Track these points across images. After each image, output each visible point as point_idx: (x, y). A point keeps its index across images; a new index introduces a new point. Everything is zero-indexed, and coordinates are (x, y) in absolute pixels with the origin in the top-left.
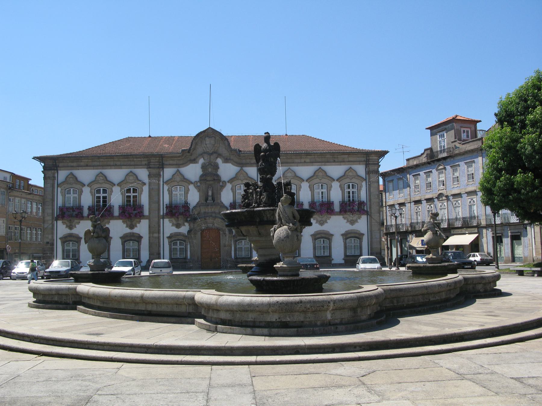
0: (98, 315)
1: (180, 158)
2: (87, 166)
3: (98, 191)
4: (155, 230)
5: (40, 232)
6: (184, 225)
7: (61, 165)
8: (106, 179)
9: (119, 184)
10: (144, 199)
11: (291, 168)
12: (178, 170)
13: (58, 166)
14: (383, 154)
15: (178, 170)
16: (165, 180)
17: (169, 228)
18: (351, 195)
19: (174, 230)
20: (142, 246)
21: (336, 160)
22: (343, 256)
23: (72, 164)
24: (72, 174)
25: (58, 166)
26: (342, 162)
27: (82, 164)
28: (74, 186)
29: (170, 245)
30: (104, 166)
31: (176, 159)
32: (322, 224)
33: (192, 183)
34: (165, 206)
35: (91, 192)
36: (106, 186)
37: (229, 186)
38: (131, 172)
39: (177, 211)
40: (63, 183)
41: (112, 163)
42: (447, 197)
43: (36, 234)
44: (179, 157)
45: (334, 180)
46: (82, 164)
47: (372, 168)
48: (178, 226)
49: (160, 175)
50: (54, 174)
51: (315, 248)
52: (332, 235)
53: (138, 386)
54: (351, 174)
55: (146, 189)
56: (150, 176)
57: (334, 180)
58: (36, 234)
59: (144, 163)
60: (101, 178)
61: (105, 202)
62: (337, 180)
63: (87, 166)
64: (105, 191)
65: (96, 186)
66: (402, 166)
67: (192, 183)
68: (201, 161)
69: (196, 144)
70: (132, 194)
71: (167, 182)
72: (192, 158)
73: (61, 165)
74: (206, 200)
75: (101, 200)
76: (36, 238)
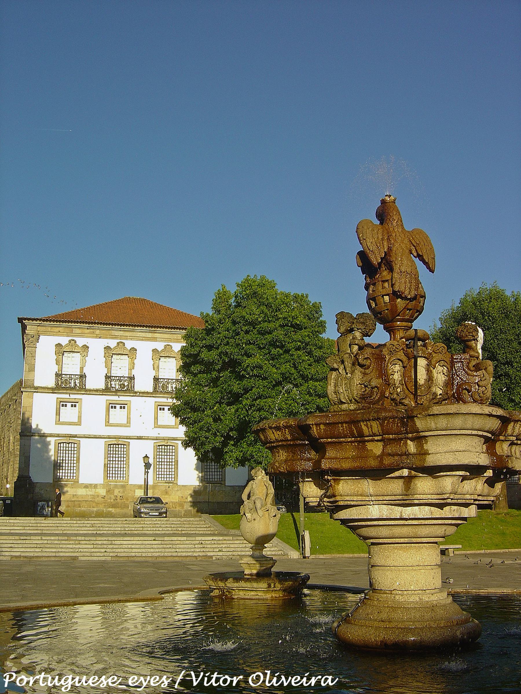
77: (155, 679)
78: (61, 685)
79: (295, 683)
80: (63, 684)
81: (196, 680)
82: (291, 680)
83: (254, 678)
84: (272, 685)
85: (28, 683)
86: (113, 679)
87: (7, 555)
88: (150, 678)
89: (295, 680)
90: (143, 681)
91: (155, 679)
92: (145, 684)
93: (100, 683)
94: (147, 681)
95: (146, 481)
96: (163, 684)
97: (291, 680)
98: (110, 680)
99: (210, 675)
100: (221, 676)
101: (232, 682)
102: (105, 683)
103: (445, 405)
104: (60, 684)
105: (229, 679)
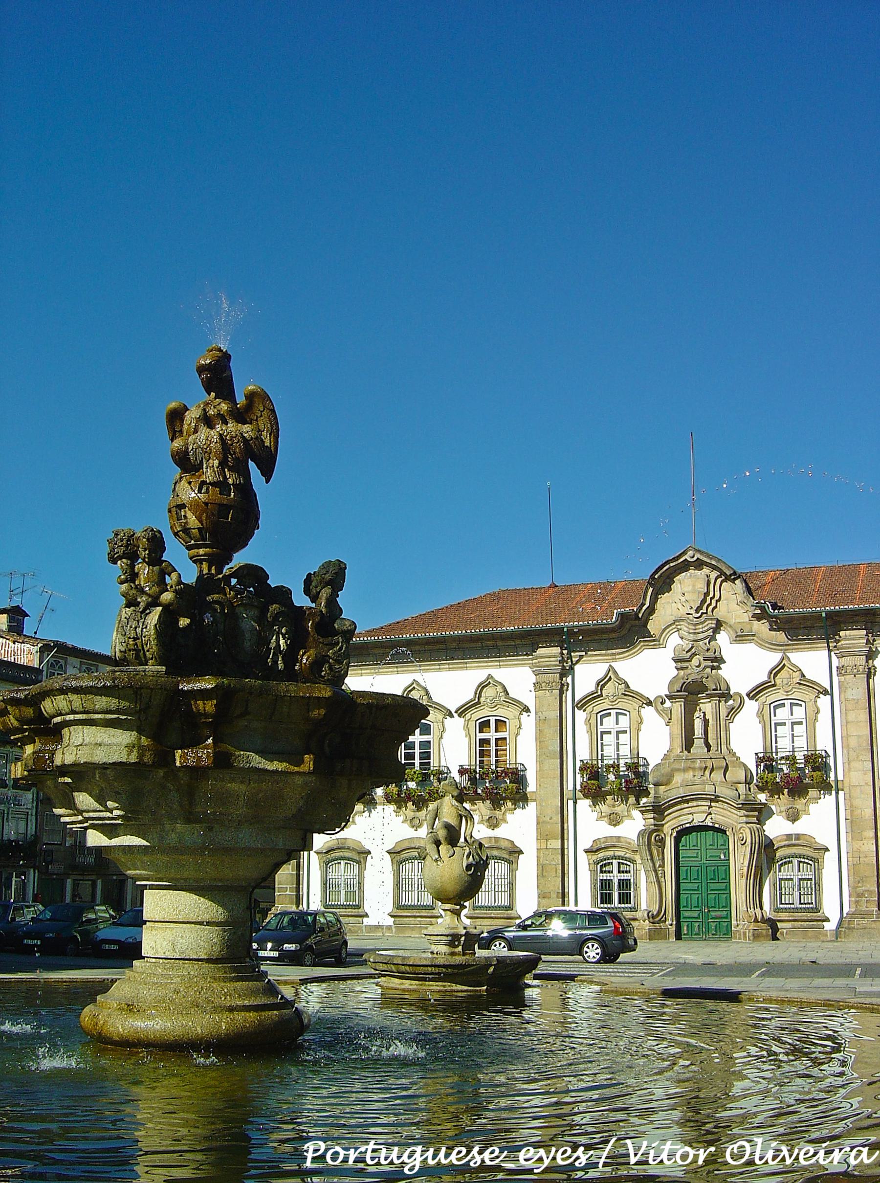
1: (614, 635)
3: (484, 725)
4: (557, 830)
6: (629, 816)
9: (462, 711)
10: (525, 751)
12: (611, 668)
15: (611, 668)
16: (577, 699)
17: (590, 824)
19: (604, 830)
20: (367, 873)
22: (389, 907)
29: (593, 872)
31: (605, 636)
32: (794, 817)
33: (649, 703)
34: (578, 764)
35: (466, 727)
36: (502, 712)
37: (751, 707)
38: (490, 676)
39: (617, 783)
44: (613, 630)
48: (615, 820)
51: (398, 885)
52: (521, 852)
55: (529, 722)
61: (426, 756)
64: (500, 724)
68: (674, 640)
70: (491, 735)
71: (581, 705)
74: (688, 744)
75: (417, 751)
77: (565, 1152)
78: (403, 1163)
79: (563, 1159)
80: (407, 1161)
81: (636, 1155)
82: (798, 1154)
83: (735, 1151)
84: (439, 1163)
85: (346, 1160)
86: (459, 1152)
87: (877, 981)
88: (557, 1151)
89: (805, 1154)
90: (545, 1157)
91: (565, 1152)
92: (547, 1162)
93: (575, 1160)
94: (550, 1158)
95: (575, 803)
96: (578, 1161)
97: (798, 1154)
98: (487, 1155)
99: (659, 1145)
100: (679, 1147)
101: (696, 1157)
102: (478, 1159)
103: (766, 573)
104: (448, 1160)
105: (342, 1153)
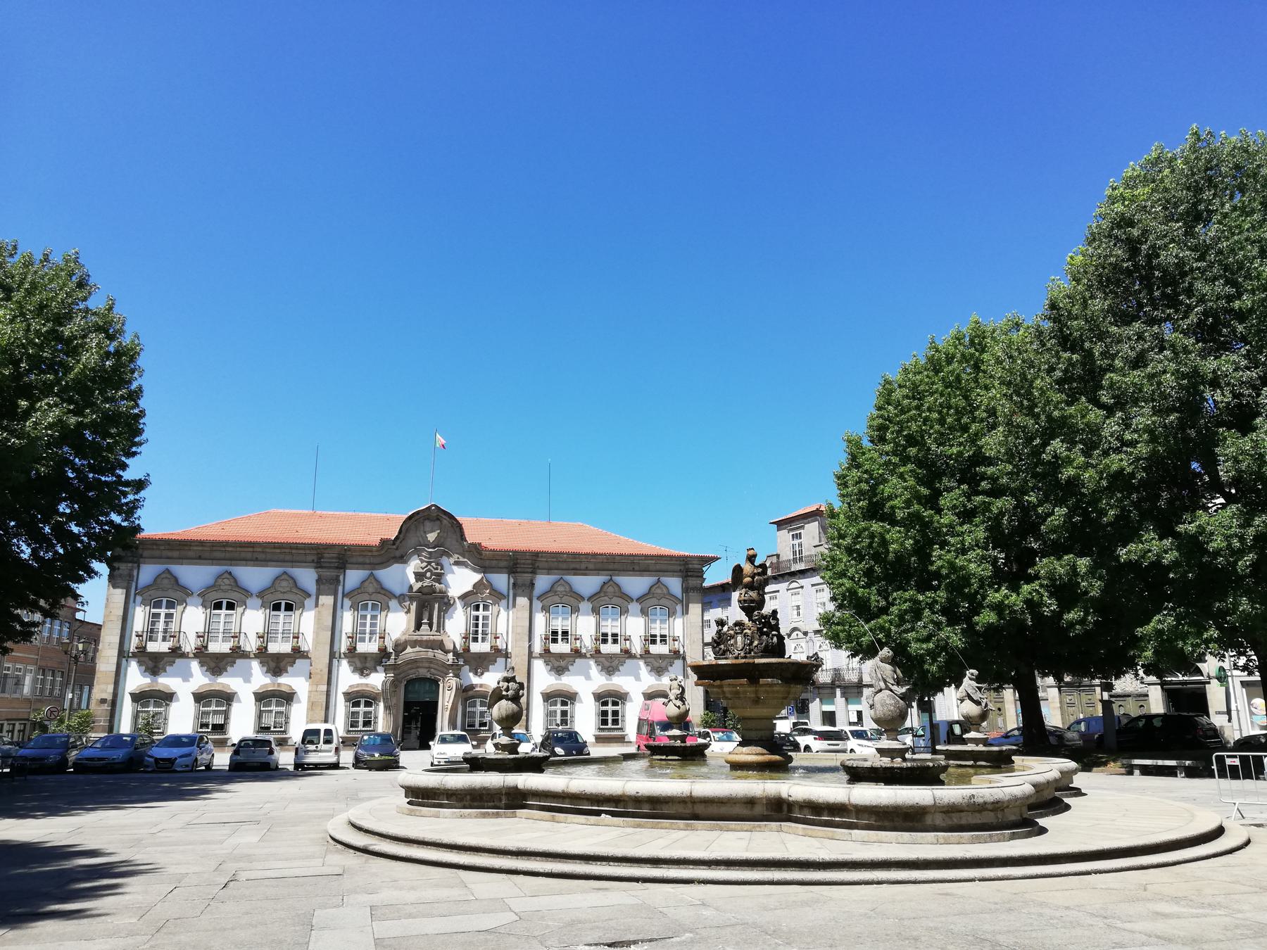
0: (639, 826)
2: (200, 558)
5: (59, 679)
6: (376, 671)
7: (146, 553)
8: (236, 585)
11: (662, 579)
13: (141, 556)
14: (709, 560)
18: (480, 622)
21: (637, 568)
23: (170, 554)
24: (168, 571)
25: (141, 556)
26: (213, 560)
27: (190, 554)
28: (171, 593)
30: (171, 560)
33: (395, 597)
40: (148, 587)
41: (249, 556)
42: (805, 634)
43: (53, 682)
45: (583, 599)
46: (190, 554)
47: (693, 582)
49: (338, 581)
50: (131, 570)
53: (1240, 911)
54: (659, 591)
56: (319, 581)
57: (583, 599)
58: (53, 682)
59: (310, 558)
60: (227, 581)
62: (638, 600)
63: (585, 571)
65: (269, 597)
66: (725, 581)
67: (395, 597)
69: (407, 530)
72: (398, 553)
73: (146, 553)
76: (52, 690)
